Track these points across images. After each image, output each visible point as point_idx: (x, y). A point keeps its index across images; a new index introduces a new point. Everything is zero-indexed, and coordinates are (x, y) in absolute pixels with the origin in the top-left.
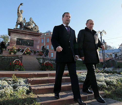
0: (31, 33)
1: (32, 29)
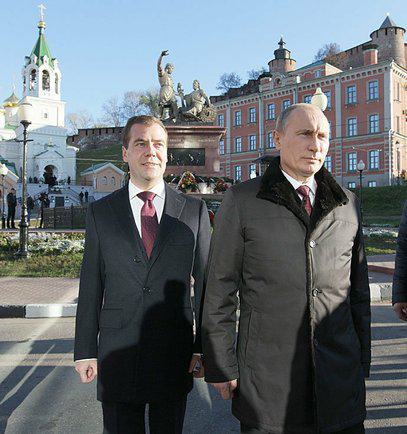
0: (195, 129)
1: (198, 114)
